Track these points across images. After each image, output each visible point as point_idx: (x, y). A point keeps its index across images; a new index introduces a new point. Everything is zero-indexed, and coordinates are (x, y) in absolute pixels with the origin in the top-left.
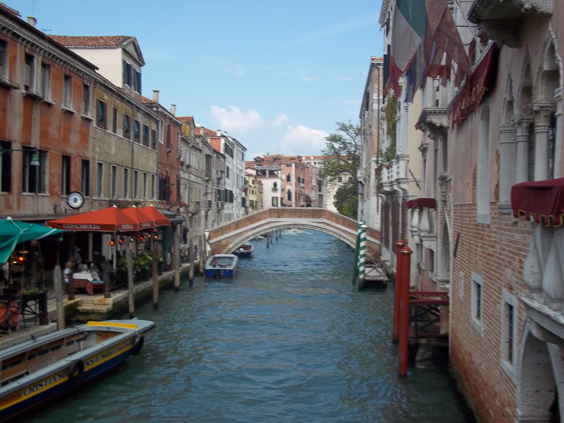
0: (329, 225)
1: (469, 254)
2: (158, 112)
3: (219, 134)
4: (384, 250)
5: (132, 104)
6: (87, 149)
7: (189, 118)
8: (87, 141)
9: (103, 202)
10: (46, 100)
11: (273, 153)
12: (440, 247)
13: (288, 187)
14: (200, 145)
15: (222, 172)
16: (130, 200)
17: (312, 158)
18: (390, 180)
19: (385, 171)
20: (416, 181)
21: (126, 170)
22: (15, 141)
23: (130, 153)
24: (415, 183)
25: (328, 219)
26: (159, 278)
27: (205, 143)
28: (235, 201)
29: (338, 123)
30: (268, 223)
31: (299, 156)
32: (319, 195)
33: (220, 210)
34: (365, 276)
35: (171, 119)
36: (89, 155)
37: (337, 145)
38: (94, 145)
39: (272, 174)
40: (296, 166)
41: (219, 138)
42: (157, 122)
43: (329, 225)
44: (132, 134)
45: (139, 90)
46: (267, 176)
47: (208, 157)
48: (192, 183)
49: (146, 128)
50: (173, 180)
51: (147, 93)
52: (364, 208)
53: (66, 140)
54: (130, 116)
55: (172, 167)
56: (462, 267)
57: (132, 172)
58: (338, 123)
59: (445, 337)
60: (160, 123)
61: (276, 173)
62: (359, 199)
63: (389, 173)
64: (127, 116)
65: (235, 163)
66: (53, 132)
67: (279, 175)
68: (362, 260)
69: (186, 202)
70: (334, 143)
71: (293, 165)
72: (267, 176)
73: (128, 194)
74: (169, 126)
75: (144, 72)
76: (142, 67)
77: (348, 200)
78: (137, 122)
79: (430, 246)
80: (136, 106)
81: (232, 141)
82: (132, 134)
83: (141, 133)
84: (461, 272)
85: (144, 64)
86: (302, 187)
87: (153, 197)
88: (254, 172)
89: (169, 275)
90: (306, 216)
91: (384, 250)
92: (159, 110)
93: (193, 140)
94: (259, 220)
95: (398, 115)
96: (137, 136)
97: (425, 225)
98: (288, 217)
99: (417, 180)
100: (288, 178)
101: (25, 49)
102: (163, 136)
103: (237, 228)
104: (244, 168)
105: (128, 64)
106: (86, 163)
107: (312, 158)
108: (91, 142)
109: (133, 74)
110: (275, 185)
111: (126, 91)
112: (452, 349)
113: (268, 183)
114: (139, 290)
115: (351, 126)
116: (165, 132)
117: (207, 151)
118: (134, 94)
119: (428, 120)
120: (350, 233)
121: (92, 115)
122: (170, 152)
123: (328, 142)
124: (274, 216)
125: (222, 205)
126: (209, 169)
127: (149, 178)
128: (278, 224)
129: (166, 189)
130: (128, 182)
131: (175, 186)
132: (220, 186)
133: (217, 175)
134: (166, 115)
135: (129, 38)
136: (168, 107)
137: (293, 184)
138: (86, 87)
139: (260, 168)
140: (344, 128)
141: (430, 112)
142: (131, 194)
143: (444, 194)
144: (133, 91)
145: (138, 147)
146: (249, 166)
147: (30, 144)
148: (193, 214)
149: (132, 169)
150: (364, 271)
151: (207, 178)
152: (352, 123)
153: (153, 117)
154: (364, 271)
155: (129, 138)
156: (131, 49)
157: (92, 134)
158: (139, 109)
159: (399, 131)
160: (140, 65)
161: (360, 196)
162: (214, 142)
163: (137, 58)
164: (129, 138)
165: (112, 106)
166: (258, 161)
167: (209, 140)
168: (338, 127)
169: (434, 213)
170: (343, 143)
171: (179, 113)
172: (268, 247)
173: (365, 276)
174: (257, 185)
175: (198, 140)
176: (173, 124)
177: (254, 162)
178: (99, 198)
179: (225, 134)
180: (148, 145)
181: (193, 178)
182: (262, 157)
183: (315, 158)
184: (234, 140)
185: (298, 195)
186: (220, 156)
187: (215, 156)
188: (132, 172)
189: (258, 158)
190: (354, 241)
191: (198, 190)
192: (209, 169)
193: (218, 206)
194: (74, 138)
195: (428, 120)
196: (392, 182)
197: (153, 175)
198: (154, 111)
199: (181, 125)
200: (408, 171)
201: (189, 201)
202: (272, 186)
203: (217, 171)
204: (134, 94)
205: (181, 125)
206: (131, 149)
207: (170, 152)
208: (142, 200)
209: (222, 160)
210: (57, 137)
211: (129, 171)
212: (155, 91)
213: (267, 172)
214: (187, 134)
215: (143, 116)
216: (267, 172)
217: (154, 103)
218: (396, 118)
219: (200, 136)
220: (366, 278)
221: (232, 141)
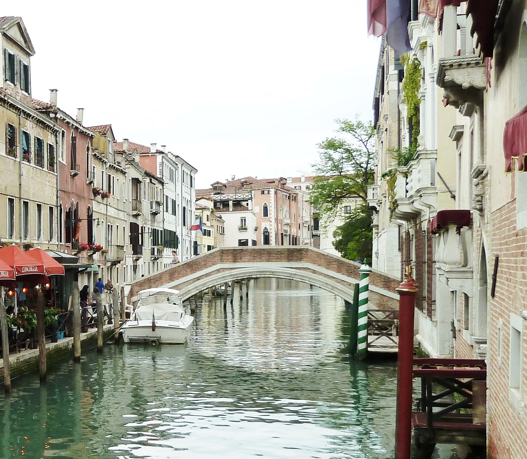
0: (314, 272)
1: (508, 286)
2: (56, 119)
3: (153, 150)
5: (17, 109)
7: (105, 127)
11: (241, 176)
13: (265, 224)
14: (123, 164)
15: (158, 203)
16: (18, 241)
17: (303, 179)
18: (409, 195)
19: (400, 180)
20: (451, 192)
21: (11, 201)
23: (17, 176)
24: (449, 194)
26: (51, 346)
27: (132, 162)
28: (180, 245)
29: (338, 121)
30: (218, 271)
31: (281, 179)
32: (313, 236)
34: (369, 345)
35: (77, 128)
39: (238, 204)
40: (276, 193)
41: (154, 155)
42: (55, 133)
43: (314, 272)
44: (19, 152)
45: (27, 89)
46: (231, 208)
47: (136, 182)
48: (112, 220)
49: (39, 142)
50: (83, 214)
51: (40, 93)
54: (16, 125)
55: (80, 197)
56: (501, 310)
58: (338, 121)
59: (481, 431)
61: (244, 203)
62: (374, 236)
63: (407, 184)
64: (11, 127)
65: (179, 191)
67: (250, 207)
68: (362, 321)
69: (103, 245)
70: (331, 152)
71: (272, 191)
72: (231, 209)
74: (74, 139)
75: (35, 64)
76: (31, 57)
77: (357, 239)
79: (461, 286)
80: (25, 113)
81: (174, 159)
82: (19, 152)
83: (32, 149)
84: (500, 319)
86: (287, 224)
88: (211, 205)
89: (68, 343)
92: (58, 116)
93: (111, 157)
94: (206, 266)
95: (421, 90)
96: (26, 153)
97: (457, 255)
98: (249, 261)
99: (451, 190)
100: (266, 210)
102: (65, 153)
104: (194, 199)
105: (10, 55)
107: (303, 179)
109: (17, 68)
110: (243, 220)
111: (8, 92)
112: (490, 447)
113: (231, 219)
114: (22, 359)
115: (360, 125)
116: (67, 146)
117: (133, 173)
118: (20, 94)
119: (447, 78)
122: (75, 175)
123: (323, 151)
125: (160, 252)
126: (137, 200)
127: (45, 211)
128: (234, 272)
129: (71, 225)
131: (86, 221)
132: (156, 224)
133: (152, 208)
134: (68, 123)
136: (73, 114)
137: (273, 220)
139: (218, 197)
140: (349, 128)
141: (451, 66)
142: (20, 234)
143: (479, 198)
144: (19, 91)
145: (29, 169)
146: (201, 195)
148: (114, 263)
149: (20, 198)
150: (365, 339)
151: (135, 213)
152: (359, 119)
153: (48, 126)
154: (365, 339)
155: (15, 156)
156: (14, 33)
158: (28, 115)
159: (424, 115)
160: (29, 55)
161: (374, 230)
162: (147, 161)
163: (23, 45)
164: (15, 156)
166: (218, 188)
167: (137, 159)
168: (338, 126)
169: (470, 232)
170: (347, 151)
171: (89, 122)
174: (215, 223)
175: (119, 158)
176: (80, 134)
177: (211, 189)
179: (161, 149)
180: (42, 166)
181: (112, 212)
182: (224, 182)
183: (308, 179)
184: (177, 157)
185: (280, 237)
186: (154, 181)
187: (148, 180)
188: (20, 203)
190: (352, 293)
191: (121, 229)
192: (137, 200)
193: (153, 253)
195: (447, 78)
196: (411, 197)
198: (51, 119)
199: (92, 137)
200: (436, 175)
201: (108, 242)
202: (239, 224)
204: (20, 94)
205: (92, 137)
206: (17, 171)
207: (75, 175)
208: (35, 242)
209: (160, 187)
211: (16, 201)
212: (52, 91)
213: (231, 203)
214: (101, 149)
215: (35, 126)
216: (231, 203)
217: (51, 107)
218: (419, 96)
219: (122, 153)
220: (370, 349)
221: (174, 159)
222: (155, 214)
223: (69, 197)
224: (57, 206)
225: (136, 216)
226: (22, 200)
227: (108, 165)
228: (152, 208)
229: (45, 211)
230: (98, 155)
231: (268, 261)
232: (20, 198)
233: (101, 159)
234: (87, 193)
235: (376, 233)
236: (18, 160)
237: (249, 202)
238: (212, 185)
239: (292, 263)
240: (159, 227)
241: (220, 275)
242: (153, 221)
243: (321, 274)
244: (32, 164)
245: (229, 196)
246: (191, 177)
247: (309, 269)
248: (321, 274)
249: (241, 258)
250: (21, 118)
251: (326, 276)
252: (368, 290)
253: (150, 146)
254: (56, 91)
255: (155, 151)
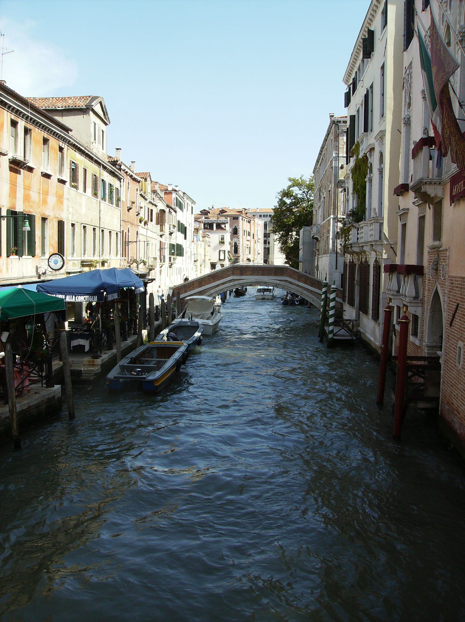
4: (346, 307)
6: (62, 210)
8: (62, 203)
9: (76, 262)
10: (28, 164)
12: (427, 315)
21: (94, 229)
22: (3, 206)
25: (290, 276)
29: (290, 180)
30: (231, 281)
33: (172, 265)
36: (63, 217)
37: (288, 201)
38: (68, 206)
42: (119, 179)
52: (319, 264)
53: (45, 202)
54: (98, 175)
57: (99, 231)
58: (290, 180)
60: (122, 180)
63: (358, 234)
66: (34, 195)
73: (97, 253)
78: (103, 180)
80: (103, 166)
85: (110, 123)
87: (117, 254)
90: (269, 274)
91: (346, 307)
93: (149, 195)
94: (223, 278)
101: (11, 116)
103: (200, 286)
106: (61, 224)
108: (65, 202)
118: (100, 153)
120: (312, 291)
121: (66, 176)
124: (237, 274)
127: (114, 235)
128: (241, 282)
130: (97, 241)
132: (172, 240)
133: (170, 229)
135: (97, 97)
138: (61, 149)
140: (296, 183)
145: (105, 205)
147: (15, 208)
157: (66, 196)
165: (83, 167)
172: (230, 303)
173: (334, 335)
178: (73, 259)
179: (177, 189)
186: (171, 211)
189: (204, 210)
193: (170, 261)
194: (52, 200)
197: (117, 233)
203: (170, 225)
209: (173, 213)
210: (37, 200)
211: (97, 229)
212: (117, 149)
215: (108, 175)
222: (171, 234)
223: (126, 225)
224: (120, 232)
225: (161, 236)
226: (101, 229)
227: (148, 201)
228: (170, 229)
229: (114, 235)
230: (143, 194)
231: (263, 275)
232: (100, 228)
233: (144, 197)
234: (136, 221)
235: (125, 170)
236: (99, 200)
237: (227, 225)
238: (201, 212)
239: (277, 277)
240: (174, 242)
241: (231, 284)
242: (170, 239)
243: (294, 284)
244: (107, 202)
245: (213, 218)
246: (192, 207)
247: (287, 281)
248: (294, 284)
249: (245, 273)
250: (101, 170)
251: (297, 285)
252: (335, 300)
253: (168, 185)
254: (120, 149)
255: (171, 189)
